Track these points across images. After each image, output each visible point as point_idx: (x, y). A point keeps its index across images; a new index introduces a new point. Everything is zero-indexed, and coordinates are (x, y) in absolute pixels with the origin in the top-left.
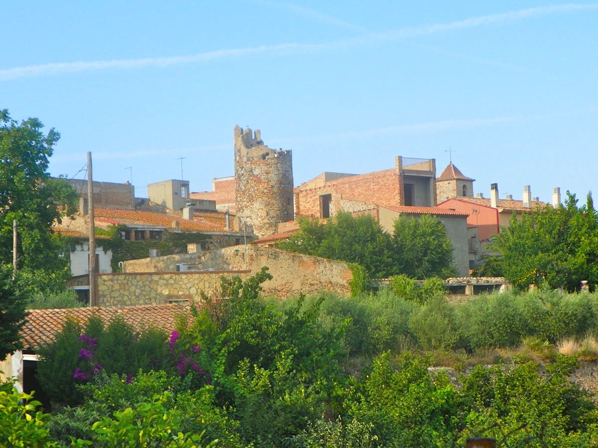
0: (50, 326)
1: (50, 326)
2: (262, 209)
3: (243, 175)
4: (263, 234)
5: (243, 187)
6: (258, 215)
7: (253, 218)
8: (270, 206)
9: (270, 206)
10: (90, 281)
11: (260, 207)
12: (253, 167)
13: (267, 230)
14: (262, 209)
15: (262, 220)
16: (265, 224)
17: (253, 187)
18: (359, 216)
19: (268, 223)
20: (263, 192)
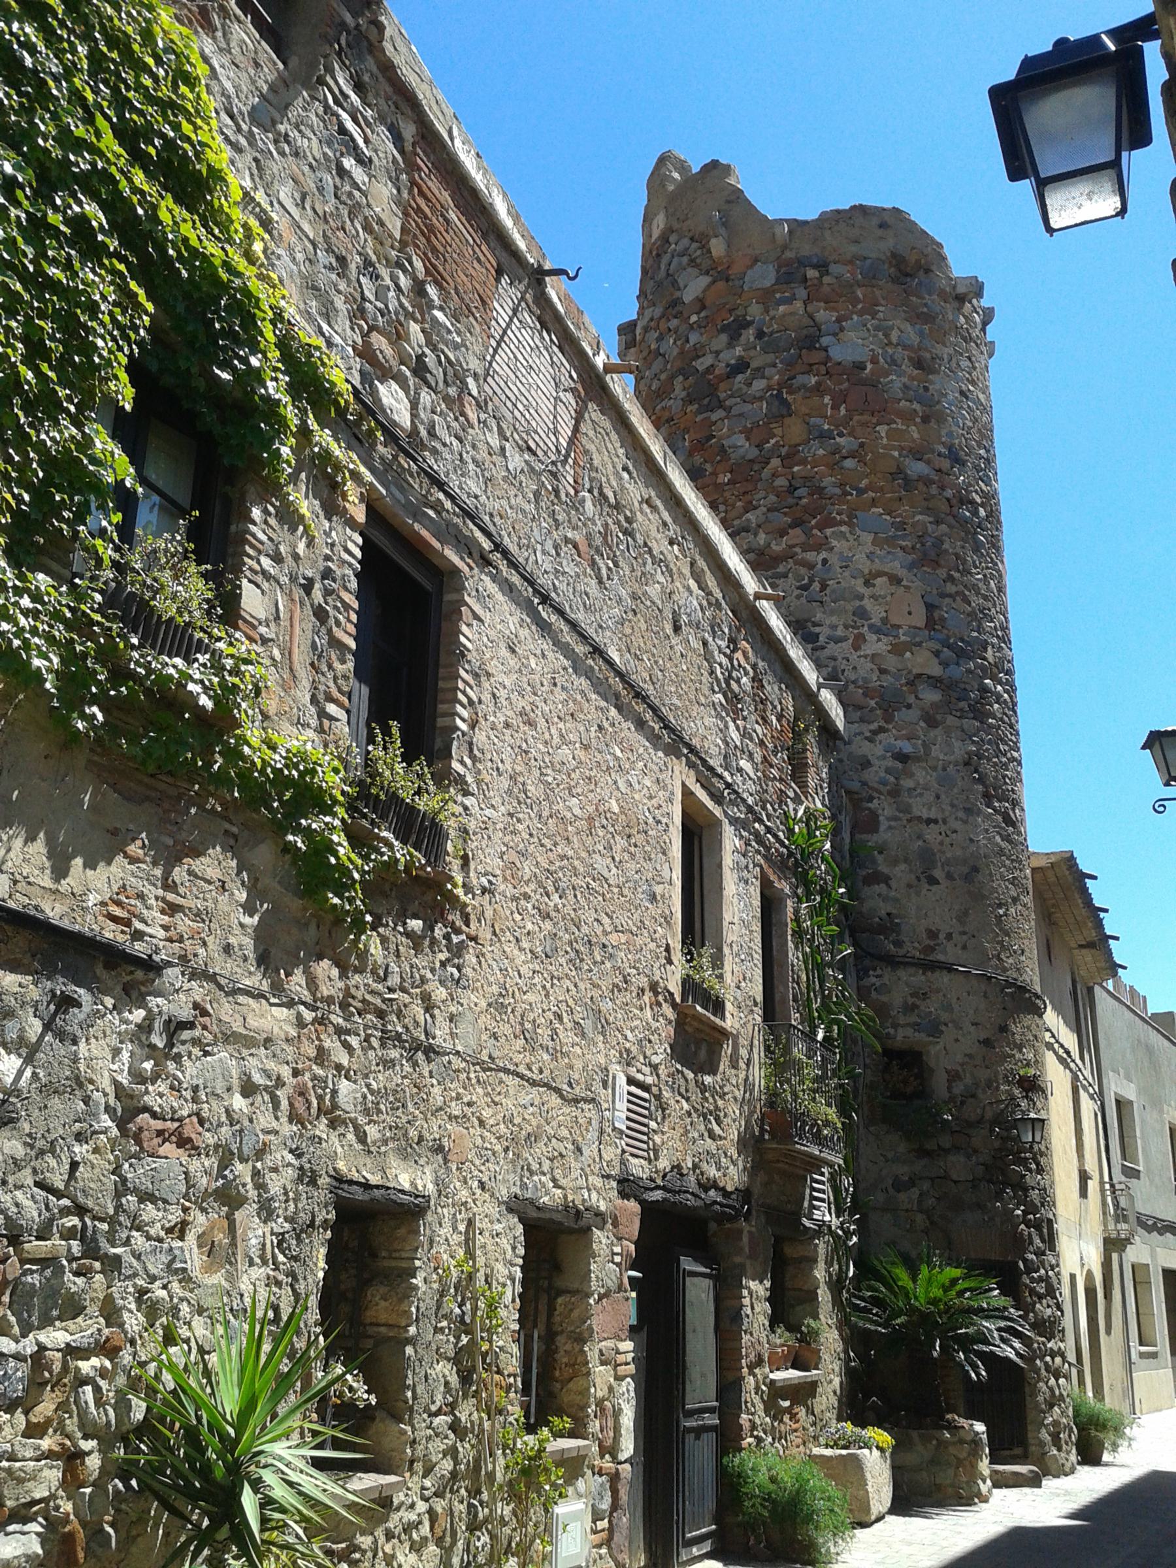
0: (588, 649)
1: (588, 649)
2: (895, 580)
3: (741, 366)
4: (907, 748)
5: (740, 440)
6: (862, 613)
7: (824, 632)
8: (942, 573)
9: (942, 573)
10: (477, 177)
11: (878, 566)
12: (824, 315)
13: (932, 723)
14: (895, 580)
15: (897, 650)
16: (914, 681)
17: (824, 436)
18: (170, 854)
19: (935, 682)
20: (899, 472)
